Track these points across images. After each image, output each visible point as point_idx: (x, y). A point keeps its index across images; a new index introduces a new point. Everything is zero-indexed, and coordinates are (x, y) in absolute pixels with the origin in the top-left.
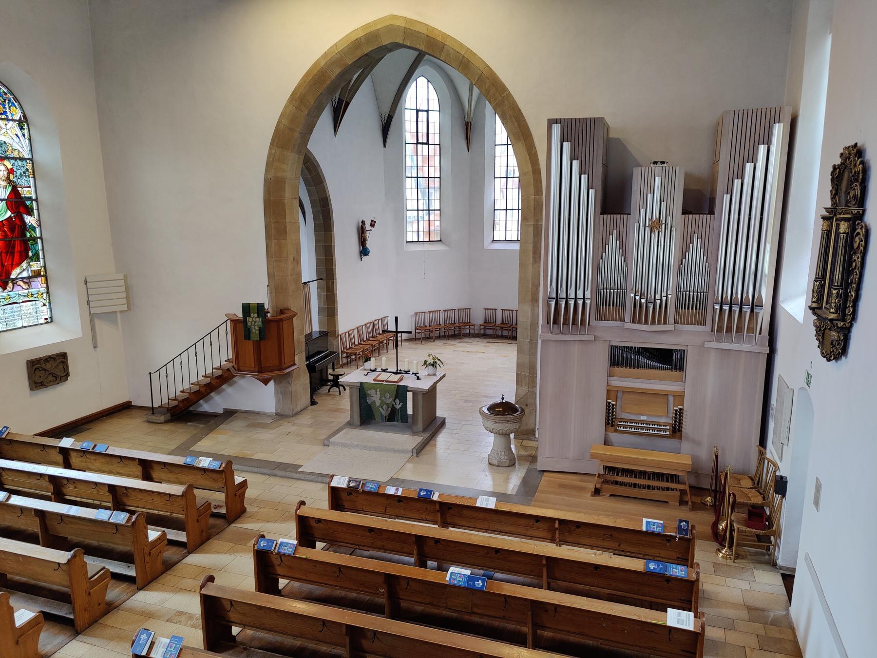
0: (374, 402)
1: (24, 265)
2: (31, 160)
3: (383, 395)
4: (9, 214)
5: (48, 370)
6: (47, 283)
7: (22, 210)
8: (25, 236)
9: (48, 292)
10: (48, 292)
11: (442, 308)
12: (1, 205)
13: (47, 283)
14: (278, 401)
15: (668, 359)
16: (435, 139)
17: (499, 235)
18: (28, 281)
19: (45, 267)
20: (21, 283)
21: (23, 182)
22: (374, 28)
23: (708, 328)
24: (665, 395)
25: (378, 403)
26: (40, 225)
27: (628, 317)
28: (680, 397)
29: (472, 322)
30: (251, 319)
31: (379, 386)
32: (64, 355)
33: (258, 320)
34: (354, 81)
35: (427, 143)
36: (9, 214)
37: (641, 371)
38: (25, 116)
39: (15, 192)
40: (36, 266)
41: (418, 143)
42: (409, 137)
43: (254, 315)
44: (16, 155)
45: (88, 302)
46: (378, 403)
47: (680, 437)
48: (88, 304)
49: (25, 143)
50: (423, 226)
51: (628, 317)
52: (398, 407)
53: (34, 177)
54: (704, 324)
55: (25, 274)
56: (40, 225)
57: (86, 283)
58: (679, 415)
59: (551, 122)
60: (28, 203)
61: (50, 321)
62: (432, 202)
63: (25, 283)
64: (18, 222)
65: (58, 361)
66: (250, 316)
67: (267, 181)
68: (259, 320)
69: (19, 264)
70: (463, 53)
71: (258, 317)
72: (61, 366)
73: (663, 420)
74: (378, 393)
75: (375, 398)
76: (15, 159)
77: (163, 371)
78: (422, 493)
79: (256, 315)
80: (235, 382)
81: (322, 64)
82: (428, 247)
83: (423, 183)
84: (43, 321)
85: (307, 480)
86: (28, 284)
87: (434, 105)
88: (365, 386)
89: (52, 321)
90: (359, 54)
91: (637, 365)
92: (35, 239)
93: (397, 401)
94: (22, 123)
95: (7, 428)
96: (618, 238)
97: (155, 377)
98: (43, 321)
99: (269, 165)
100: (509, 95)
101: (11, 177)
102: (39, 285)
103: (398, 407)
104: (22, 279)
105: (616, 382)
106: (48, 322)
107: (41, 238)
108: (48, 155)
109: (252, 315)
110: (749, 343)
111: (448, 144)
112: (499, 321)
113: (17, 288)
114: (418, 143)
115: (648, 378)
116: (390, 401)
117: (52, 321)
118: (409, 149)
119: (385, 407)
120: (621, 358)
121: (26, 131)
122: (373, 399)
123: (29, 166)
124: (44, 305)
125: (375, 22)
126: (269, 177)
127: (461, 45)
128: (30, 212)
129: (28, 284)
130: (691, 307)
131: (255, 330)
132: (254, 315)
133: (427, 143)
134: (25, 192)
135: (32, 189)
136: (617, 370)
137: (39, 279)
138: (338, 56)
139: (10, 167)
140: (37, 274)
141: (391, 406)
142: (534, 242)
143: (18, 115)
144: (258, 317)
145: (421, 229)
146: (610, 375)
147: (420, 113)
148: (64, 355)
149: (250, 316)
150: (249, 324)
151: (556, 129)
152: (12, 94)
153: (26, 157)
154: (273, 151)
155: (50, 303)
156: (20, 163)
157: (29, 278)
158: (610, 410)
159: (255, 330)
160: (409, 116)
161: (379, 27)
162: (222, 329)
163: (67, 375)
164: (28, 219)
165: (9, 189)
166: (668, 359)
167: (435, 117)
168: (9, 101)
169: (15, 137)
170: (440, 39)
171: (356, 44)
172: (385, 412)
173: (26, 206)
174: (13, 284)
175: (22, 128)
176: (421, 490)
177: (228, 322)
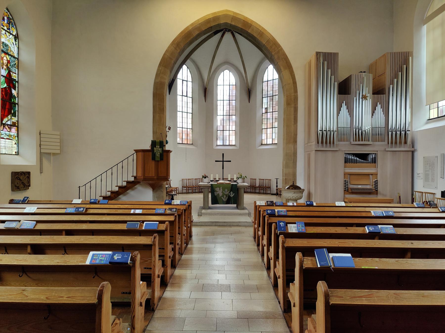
0: (219, 194)
1: (9, 117)
2: (18, 59)
3: (224, 189)
4: (5, 85)
5: (20, 180)
6: (18, 131)
7: (11, 85)
8: (11, 100)
9: (18, 137)
10: (18, 137)
11: (194, 178)
12: (3, 79)
13: (18, 131)
16: (190, 95)
17: (219, 143)
18: (10, 127)
19: (18, 121)
20: (7, 127)
21: (13, 69)
22: (218, 15)
23: (386, 142)
24: (368, 175)
25: (221, 194)
26: (18, 97)
30: (156, 149)
32: (29, 173)
33: (160, 149)
34: (191, 44)
35: (187, 96)
36: (5, 85)
37: (358, 164)
38: (17, 34)
39: (9, 74)
40: (14, 119)
41: (182, 96)
42: (179, 92)
44: (11, 53)
45: (40, 145)
46: (221, 194)
47: (377, 194)
48: (40, 147)
49: (16, 49)
52: (232, 196)
53: (18, 69)
54: (384, 141)
55: (9, 123)
56: (18, 97)
57: (40, 134)
58: (376, 183)
60: (14, 82)
61: (17, 154)
62: (266, 84)
63: (9, 127)
64: (9, 91)
65: (26, 176)
66: (156, 147)
67: (155, 83)
68: (160, 149)
69: (7, 116)
70: (260, 29)
71: (160, 148)
72: (27, 180)
73: (368, 187)
74: (221, 189)
75: (219, 192)
76: (12, 56)
77: (88, 185)
79: (159, 147)
80: (136, 188)
81: (190, 28)
82: (187, 146)
83: (185, 115)
84: (14, 153)
85: (206, 226)
86: (10, 128)
87: (190, 79)
88: (214, 186)
89: (18, 154)
90: (209, 26)
91: (356, 162)
92: (15, 104)
93: (232, 193)
94: (16, 37)
95: (28, 198)
96: (346, 105)
97: (82, 189)
98: (14, 153)
99: (157, 75)
101: (9, 65)
102: (14, 130)
103: (232, 196)
104: (8, 125)
105: (349, 170)
106: (16, 155)
107: (18, 104)
108: (28, 57)
109: (157, 146)
110: (404, 147)
111: (196, 96)
113: (5, 129)
114: (182, 96)
115: (359, 167)
116: (227, 193)
117: (18, 154)
118: (179, 98)
119: (225, 196)
121: (17, 43)
123: (16, 62)
124: (16, 144)
125: (218, 12)
126: (157, 81)
127: (260, 26)
128: (15, 89)
129: (10, 128)
131: (158, 155)
133: (187, 96)
134: (14, 76)
135: (17, 75)
136: (348, 164)
137: (15, 128)
138: (199, 25)
139: (9, 59)
140: (14, 125)
142: (294, 114)
143: (14, 33)
144: (160, 148)
145: (184, 137)
146: (345, 167)
147: (184, 81)
148: (29, 173)
149: (156, 147)
150: (155, 151)
152: (14, 20)
153: (16, 57)
154: (160, 68)
155: (18, 143)
156: (13, 59)
157: (11, 125)
158: (346, 183)
159: (158, 155)
160: (179, 82)
161: (220, 14)
162: (131, 159)
163: (29, 186)
164: (14, 92)
165: (7, 71)
167: (190, 84)
168: (12, 24)
169: (12, 44)
170: (250, 22)
171: (208, 21)
172: (225, 199)
173: (13, 84)
174: (4, 127)
175: (15, 41)
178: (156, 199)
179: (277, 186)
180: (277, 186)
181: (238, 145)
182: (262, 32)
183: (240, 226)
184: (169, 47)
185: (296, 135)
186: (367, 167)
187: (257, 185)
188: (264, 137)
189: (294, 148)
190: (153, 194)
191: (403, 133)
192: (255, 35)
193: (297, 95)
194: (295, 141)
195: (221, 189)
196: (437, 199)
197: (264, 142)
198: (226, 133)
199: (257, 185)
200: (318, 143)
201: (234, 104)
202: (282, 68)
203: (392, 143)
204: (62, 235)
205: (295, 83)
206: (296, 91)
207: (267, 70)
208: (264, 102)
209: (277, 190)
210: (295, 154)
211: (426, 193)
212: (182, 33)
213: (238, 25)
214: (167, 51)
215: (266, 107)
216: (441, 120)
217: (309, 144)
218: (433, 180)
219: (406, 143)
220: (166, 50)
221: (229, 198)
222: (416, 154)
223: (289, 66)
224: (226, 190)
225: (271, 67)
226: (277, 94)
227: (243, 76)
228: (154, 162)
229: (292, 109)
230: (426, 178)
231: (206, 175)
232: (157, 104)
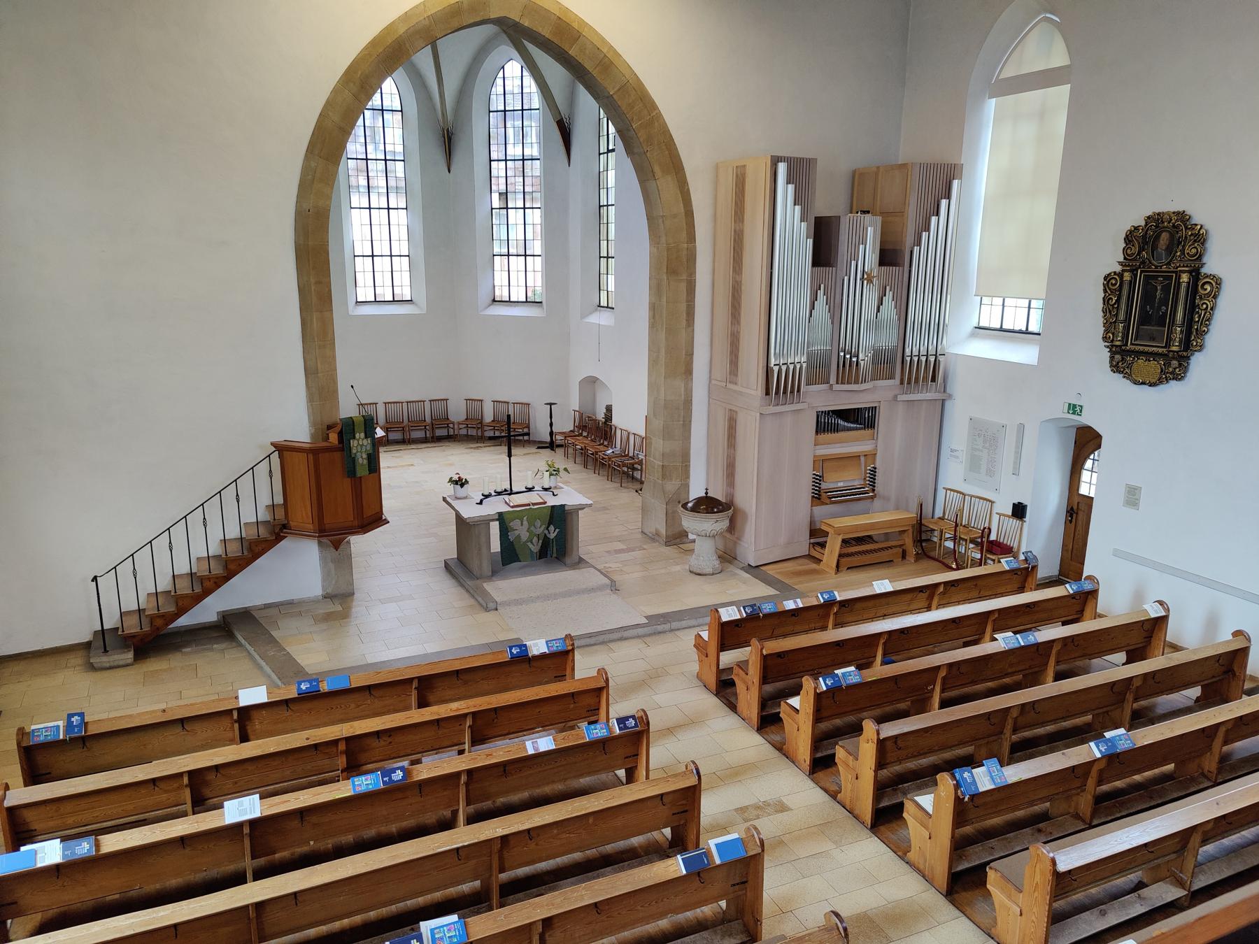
0: (519, 536)
3: (531, 524)
11: (427, 397)
14: (326, 576)
15: (861, 418)
17: (365, 293)
24: (855, 458)
25: (525, 536)
27: (833, 380)
28: (871, 456)
29: (452, 418)
31: (528, 513)
33: (365, 442)
43: (360, 435)
50: (383, 279)
51: (833, 380)
52: (552, 536)
58: (874, 470)
59: (775, 161)
70: (605, 51)
74: (525, 523)
75: (521, 531)
78: (514, 651)
79: (363, 435)
81: (402, 30)
88: (506, 517)
93: (552, 528)
97: (106, 583)
100: (659, 115)
103: (552, 536)
109: (357, 436)
112: (428, 420)
119: (535, 539)
120: (830, 422)
122: (517, 533)
127: (603, 40)
130: (885, 364)
132: (360, 435)
136: (823, 437)
138: (427, 22)
141: (542, 537)
151: (782, 168)
158: (818, 479)
162: (263, 468)
166: (861, 418)
170: (575, 25)
172: (535, 547)
176: (511, 648)
177: (275, 456)
178: (331, 566)
179: (551, 425)
180: (551, 425)
181: (422, 299)
182: (608, 62)
183: (626, 639)
184: (335, 91)
185: (690, 355)
186: (857, 440)
187: (488, 418)
188: (500, 278)
189: (686, 389)
190: (321, 552)
191: (932, 359)
192: (588, 65)
193: (695, 247)
194: (689, 372)
195: (525, 523)
196: (1000, 515)
197: (502, 293)
198: (382, 264)
199: (488, 418)
200: (767, 393)
201: (401, 174)
202: (657, 169)
203: (925, 378)
204: (490, 909)
205: (689, 214)
206: (692, 237)
207: (499, 82)
208: (494, 173)
209: (551, 433)
210: (688, 402)
211: (972, 496)
212: (374, 43)
213: (540, 30)
214: (329, 104)
215: (503, 188)
216: (1004, 339)
217: (730, 386)
218: (990, 473)
219: (933, 379)
220: (328, 102)
221: (546, 543)
222: (948, 404)
223: (675, 167)
224: (538, 523)
225: (514, 68)
226: (536, 153)
227: (430, 97)
228: (347, 481)
229: (683, 286)
230: (973, 464)
231: (464, 477)
232: (312, 280)
